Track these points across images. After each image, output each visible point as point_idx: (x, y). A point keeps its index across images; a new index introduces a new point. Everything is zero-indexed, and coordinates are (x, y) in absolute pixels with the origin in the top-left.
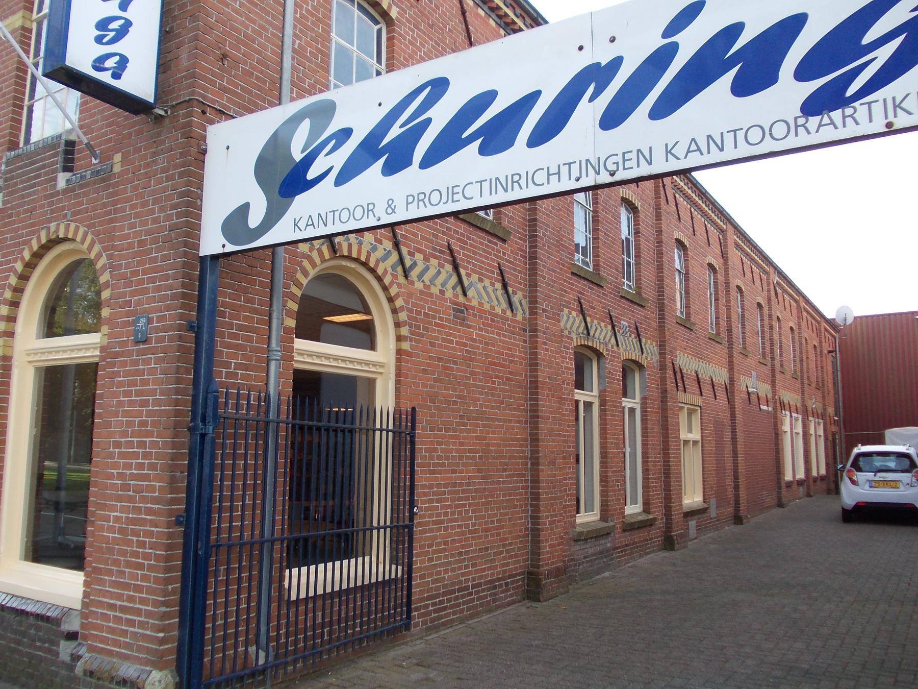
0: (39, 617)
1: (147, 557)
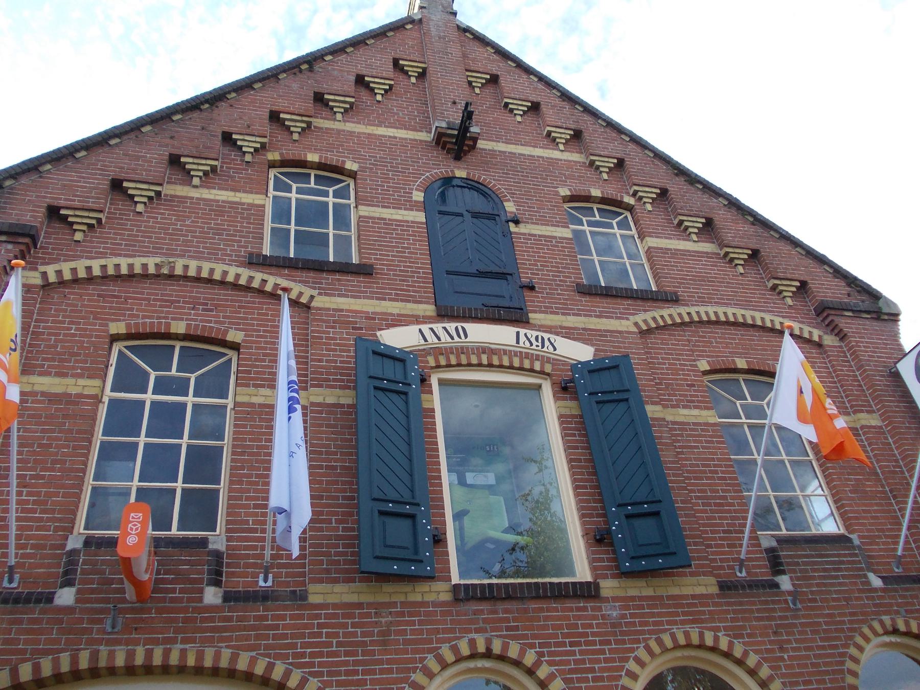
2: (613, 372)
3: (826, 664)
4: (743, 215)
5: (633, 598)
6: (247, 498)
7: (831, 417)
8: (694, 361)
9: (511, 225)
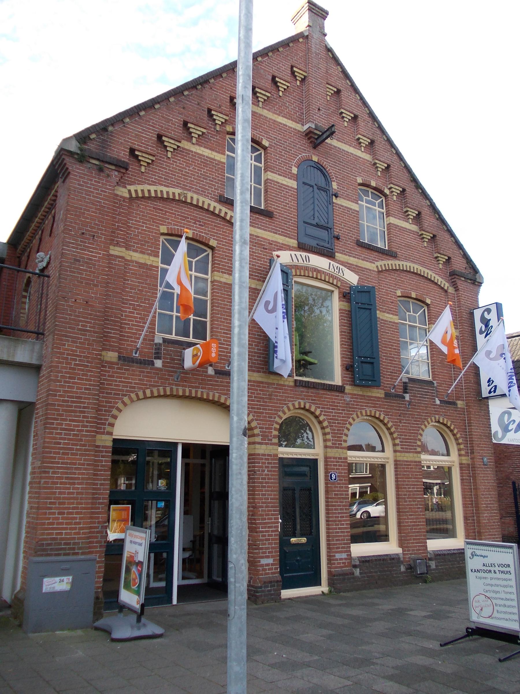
0: (289, 599)
1: (496, 525)
2: (367, 294)
3: (413, 430)
4: (435, 213)
5: (355, 395)
6: (221, 329)
7: (454, 348)
8: (396, 290)
9: (334, 197)
